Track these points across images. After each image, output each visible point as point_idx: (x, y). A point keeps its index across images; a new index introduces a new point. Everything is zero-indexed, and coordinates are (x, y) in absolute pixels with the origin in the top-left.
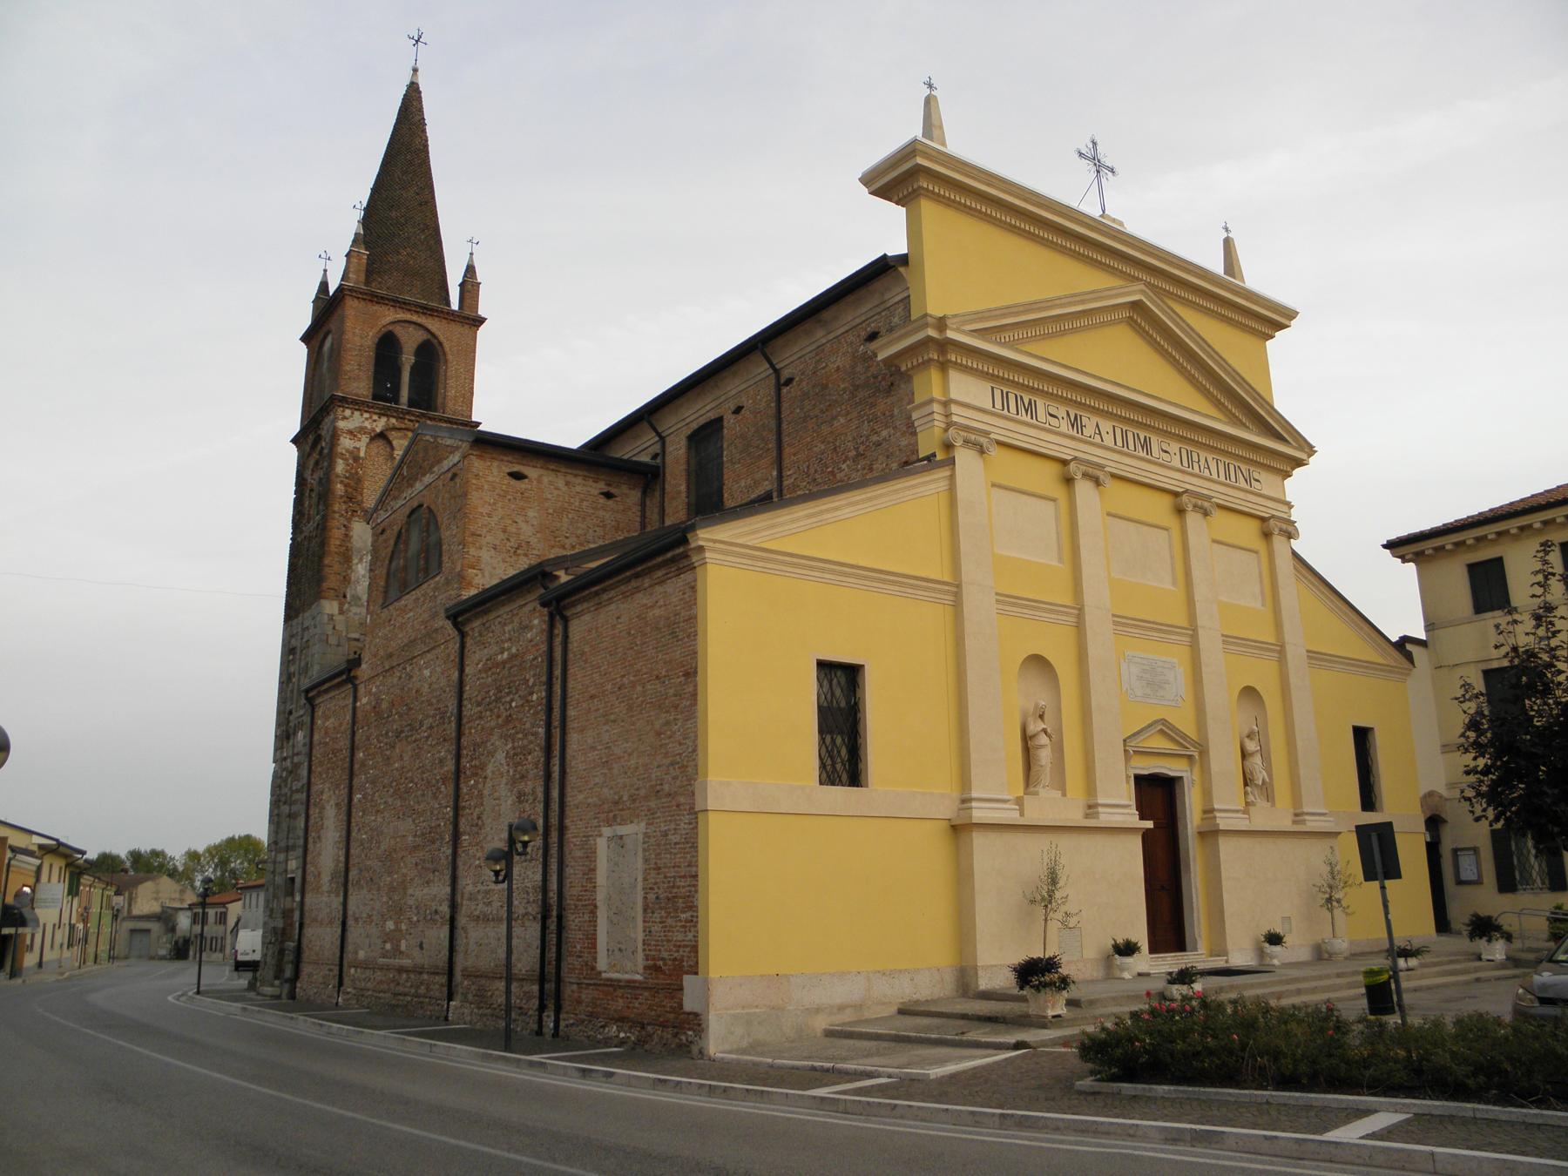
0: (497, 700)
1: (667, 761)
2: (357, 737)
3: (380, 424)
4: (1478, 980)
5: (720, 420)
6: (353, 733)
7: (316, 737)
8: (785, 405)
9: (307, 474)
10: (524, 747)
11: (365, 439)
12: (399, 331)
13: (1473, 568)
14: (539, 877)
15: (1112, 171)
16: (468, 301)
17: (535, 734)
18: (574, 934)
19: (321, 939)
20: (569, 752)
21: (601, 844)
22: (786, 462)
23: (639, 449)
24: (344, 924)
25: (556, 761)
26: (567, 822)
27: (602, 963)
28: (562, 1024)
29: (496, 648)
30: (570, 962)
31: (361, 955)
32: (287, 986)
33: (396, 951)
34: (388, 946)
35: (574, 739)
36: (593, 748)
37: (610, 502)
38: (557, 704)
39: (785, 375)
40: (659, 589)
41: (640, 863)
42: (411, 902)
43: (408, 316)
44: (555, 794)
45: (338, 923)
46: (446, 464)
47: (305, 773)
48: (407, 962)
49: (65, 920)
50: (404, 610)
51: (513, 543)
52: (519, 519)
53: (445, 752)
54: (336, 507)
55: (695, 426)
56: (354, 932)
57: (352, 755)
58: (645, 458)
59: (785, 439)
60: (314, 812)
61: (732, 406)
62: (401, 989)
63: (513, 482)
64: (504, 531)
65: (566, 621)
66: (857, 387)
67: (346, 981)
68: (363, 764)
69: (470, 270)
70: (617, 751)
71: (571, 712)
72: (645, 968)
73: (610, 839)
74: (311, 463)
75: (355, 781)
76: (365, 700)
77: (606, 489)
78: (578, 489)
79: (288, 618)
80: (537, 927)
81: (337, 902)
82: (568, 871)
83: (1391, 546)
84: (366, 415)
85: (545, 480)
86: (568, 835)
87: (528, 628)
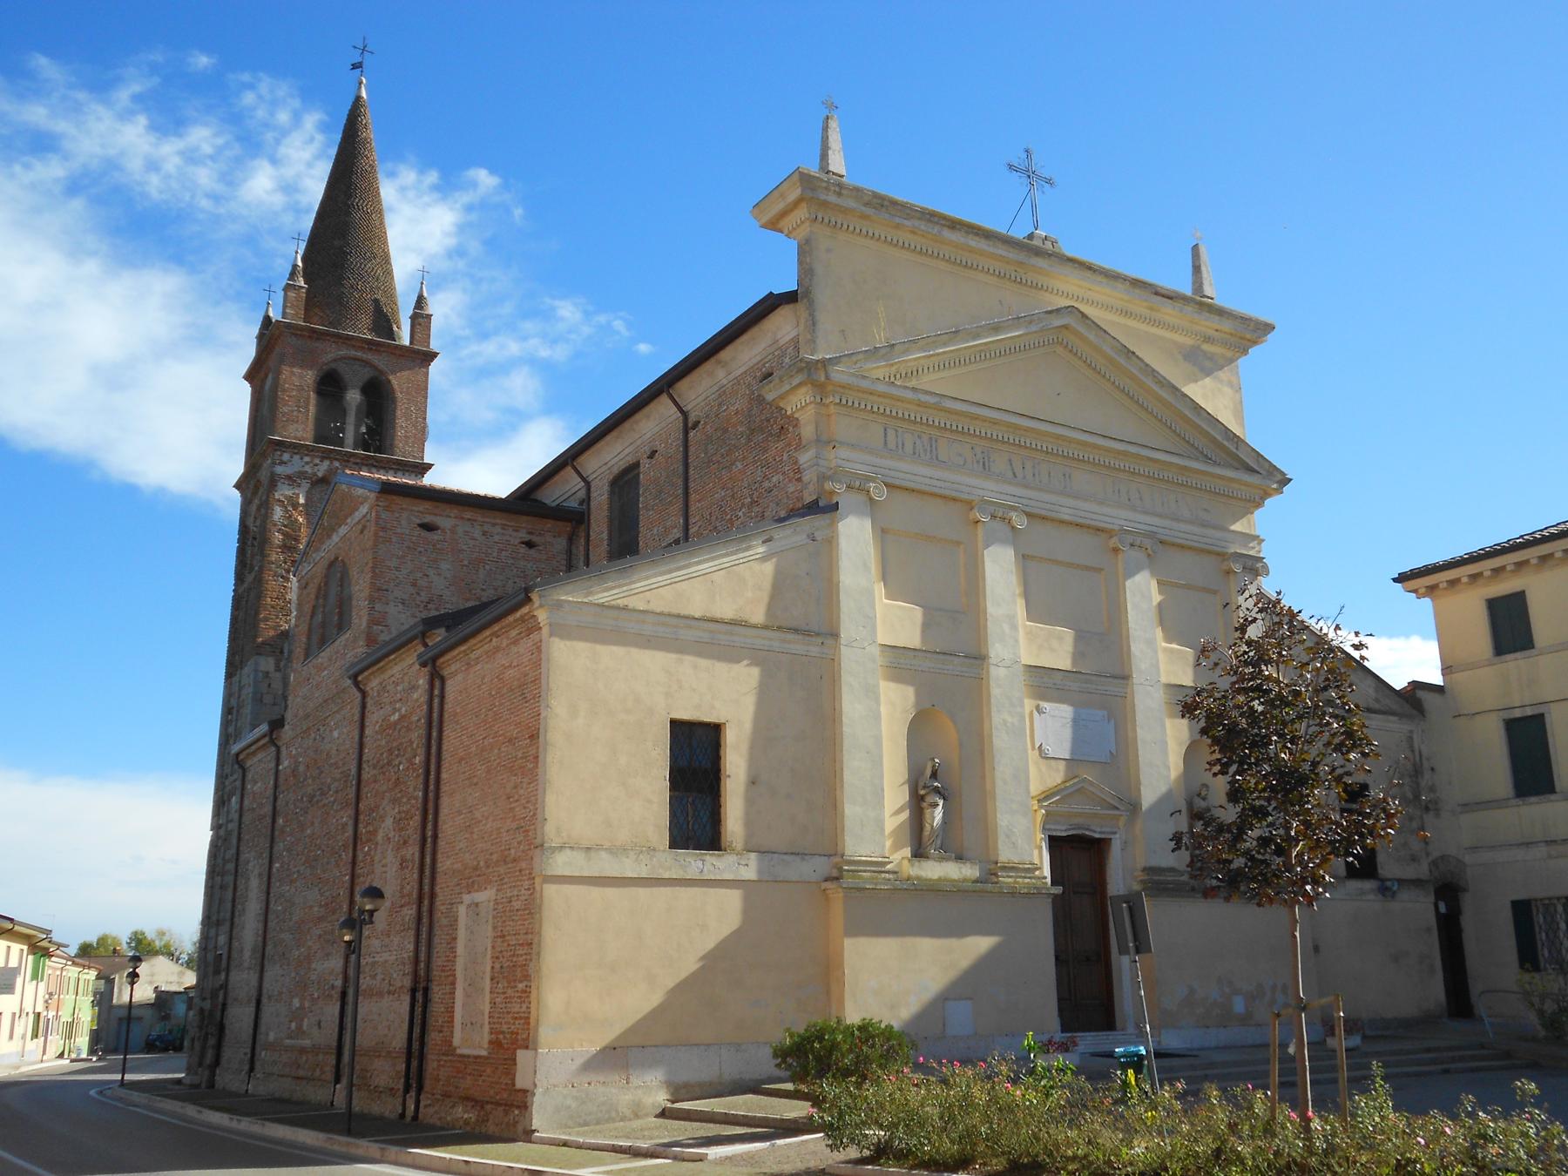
0: (389, 763)
1: (514, 825)
2: (279, 802)
3: (323, 468)
4: (1446, 1071)
5: (636, 465)
6: (275, 799)
7: (246, 802)
8: (692, 450)
9: (250, 522)
10: (407, 812)
11: (306, 485)
12: (342, 368)
13: (1493, 605)
14: (411, 947)
15: (1049, 182)
16: (418, 336)
17: (416, 798)
18: (437, 1008)
19: (239, 1017)
20: (442, 817)
21: (462, 910)
22: (692, 509)
23: (566, 489)
24: (259, 1002)
25: (430, 826)
26: (437, 889)
27: (456, 1041)
28: (422, 1104)
29: (389, 709)
30: (433, 1037)
31: (272, 1037)
32: (207, 1073)
33: (300, 1032)
34: (293, 1025)
35: (445, 802)
36: (460, 813)
37: (532, 552)
38: (433, 767)
39: (692, 419)
40: (514, 649)
41: (490, 933)
42: (313, 977)
43: (353, 353)
44: (428, 860)
45: (253, 1004)
46: (358, 515)
47: (234, 841)
48: (307, 1042)
49: (28, 1007)
50: (320, 668)
51: (424, 596)
52: (431, 572)
53: (346, 817)
54: (273, 557)
55: (616, 471)
56: (268, 1010)
57: (274, 821)
58: (573, 504)
59: (692, 485)
60: (241, 882)
61: (647, 449)
62: (301, 1073)
63: (424, 533)
64: (414, 585)
65: (443, 680)
66: (752, 431)
67: (258, 1065)
68: (283, 832)
69: (420, 302)
70: (478, 815)
71: (444, 776)
72: (490, 1042)
73: (469, 906)
74: (254, 507)
75: (276, 849)
76: (286, 763)
77: (527, 538)
78: (496, 538)
79: (229, 675)
80: (407, 999)
81: (253, 978)
82: (436, 940)
83: (1401, 579)
84: (307, 459)
85: (460, 530)
86: (438, 903)
87: (414, 688)
